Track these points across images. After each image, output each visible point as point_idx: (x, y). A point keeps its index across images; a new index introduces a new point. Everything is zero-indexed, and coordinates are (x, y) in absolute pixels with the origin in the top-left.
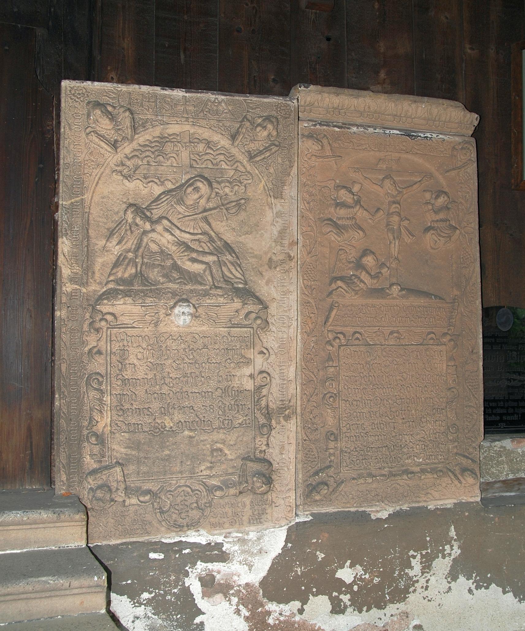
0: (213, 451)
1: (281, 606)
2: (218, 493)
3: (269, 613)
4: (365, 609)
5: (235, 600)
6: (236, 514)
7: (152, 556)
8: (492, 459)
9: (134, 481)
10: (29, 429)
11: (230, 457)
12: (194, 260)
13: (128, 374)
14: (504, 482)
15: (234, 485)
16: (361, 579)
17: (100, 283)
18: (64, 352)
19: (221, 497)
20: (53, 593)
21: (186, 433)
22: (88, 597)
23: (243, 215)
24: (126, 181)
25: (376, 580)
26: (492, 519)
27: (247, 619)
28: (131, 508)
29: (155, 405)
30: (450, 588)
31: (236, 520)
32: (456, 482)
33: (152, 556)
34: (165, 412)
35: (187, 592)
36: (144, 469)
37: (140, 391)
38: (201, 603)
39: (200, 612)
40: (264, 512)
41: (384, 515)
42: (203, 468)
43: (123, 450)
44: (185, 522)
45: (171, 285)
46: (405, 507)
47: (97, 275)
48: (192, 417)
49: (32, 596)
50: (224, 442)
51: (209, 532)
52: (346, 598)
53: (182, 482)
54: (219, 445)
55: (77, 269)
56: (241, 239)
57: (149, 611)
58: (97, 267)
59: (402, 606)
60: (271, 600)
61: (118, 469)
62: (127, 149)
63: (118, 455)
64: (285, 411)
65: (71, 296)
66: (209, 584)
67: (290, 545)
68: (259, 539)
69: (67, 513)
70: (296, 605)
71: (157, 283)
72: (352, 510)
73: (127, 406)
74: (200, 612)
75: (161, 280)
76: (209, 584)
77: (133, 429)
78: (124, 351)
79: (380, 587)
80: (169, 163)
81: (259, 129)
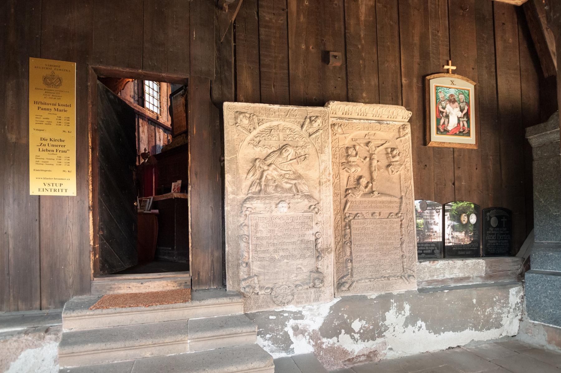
0: (297, 268)
1: (329, 339)
2: (300, 288)
3: (323, 343)
4: (366, 341)
5: (308, 337)
6: (307, 297)
7: (271, 317)
8: (421, 270)
9: (263, 283)
10: (212, 261)
11: (305, 271)
12: (287, 183)
13: (259, 235)
14: (426, 281)
15: (307, 284)
16: (364, 327)
17: (245, 194)
18: (230, 226)
19: (301, 290)
20: (234, 335)
21: (285, 261)
22: (249, 337)
23: (306, 162)
24: (255, 148)
25: (371, 327)
26: (423, 298)
27: (313, 346)
28: (262, 296)
29: (271, 249)
30: (405, 331)
31: (308, 300)
32: (406, 281)
33: (271, 317)
34: (275, 251)
35: (286, 333)
36: (267, 277)
37: (264, 242)
38: (293, 338)
39: (292, 343)
40: (320, 296)
41: (374, 297)
42: (293, 276)
43: (258, 269)
44: (286, 302)
45: (276, 194)
46: (383, 293)
47: (243, 190)
48: (288, 254)
49: (225, 336)
50: (302, 264)
51: (296, 306)
52: (357, 336)
53: (284, 283)
54: (300, 266)
55: (235, 188)
56: (307, 172)
57: (270, 343)
58: (243, 187)
59: (382, 340)
60: (324, 337)
61: (256, 278)
62: (255, 133)
63: (255, 272)
64: (327, 250)
65: (233, 200)
66: (296, 329)
67: (332, 312)
68: (318, 309)
69: (236, 299)
70: (335, 339)
71: (271, 193)
72: (359, 294)
73: (258, 249)
74: (292, 343)
75: (273, 192)
76: (296, 329)
77: (261, 259)
78: (257, 225)
79: (373, 330)
80: (274, 139)
81: (313, 122)
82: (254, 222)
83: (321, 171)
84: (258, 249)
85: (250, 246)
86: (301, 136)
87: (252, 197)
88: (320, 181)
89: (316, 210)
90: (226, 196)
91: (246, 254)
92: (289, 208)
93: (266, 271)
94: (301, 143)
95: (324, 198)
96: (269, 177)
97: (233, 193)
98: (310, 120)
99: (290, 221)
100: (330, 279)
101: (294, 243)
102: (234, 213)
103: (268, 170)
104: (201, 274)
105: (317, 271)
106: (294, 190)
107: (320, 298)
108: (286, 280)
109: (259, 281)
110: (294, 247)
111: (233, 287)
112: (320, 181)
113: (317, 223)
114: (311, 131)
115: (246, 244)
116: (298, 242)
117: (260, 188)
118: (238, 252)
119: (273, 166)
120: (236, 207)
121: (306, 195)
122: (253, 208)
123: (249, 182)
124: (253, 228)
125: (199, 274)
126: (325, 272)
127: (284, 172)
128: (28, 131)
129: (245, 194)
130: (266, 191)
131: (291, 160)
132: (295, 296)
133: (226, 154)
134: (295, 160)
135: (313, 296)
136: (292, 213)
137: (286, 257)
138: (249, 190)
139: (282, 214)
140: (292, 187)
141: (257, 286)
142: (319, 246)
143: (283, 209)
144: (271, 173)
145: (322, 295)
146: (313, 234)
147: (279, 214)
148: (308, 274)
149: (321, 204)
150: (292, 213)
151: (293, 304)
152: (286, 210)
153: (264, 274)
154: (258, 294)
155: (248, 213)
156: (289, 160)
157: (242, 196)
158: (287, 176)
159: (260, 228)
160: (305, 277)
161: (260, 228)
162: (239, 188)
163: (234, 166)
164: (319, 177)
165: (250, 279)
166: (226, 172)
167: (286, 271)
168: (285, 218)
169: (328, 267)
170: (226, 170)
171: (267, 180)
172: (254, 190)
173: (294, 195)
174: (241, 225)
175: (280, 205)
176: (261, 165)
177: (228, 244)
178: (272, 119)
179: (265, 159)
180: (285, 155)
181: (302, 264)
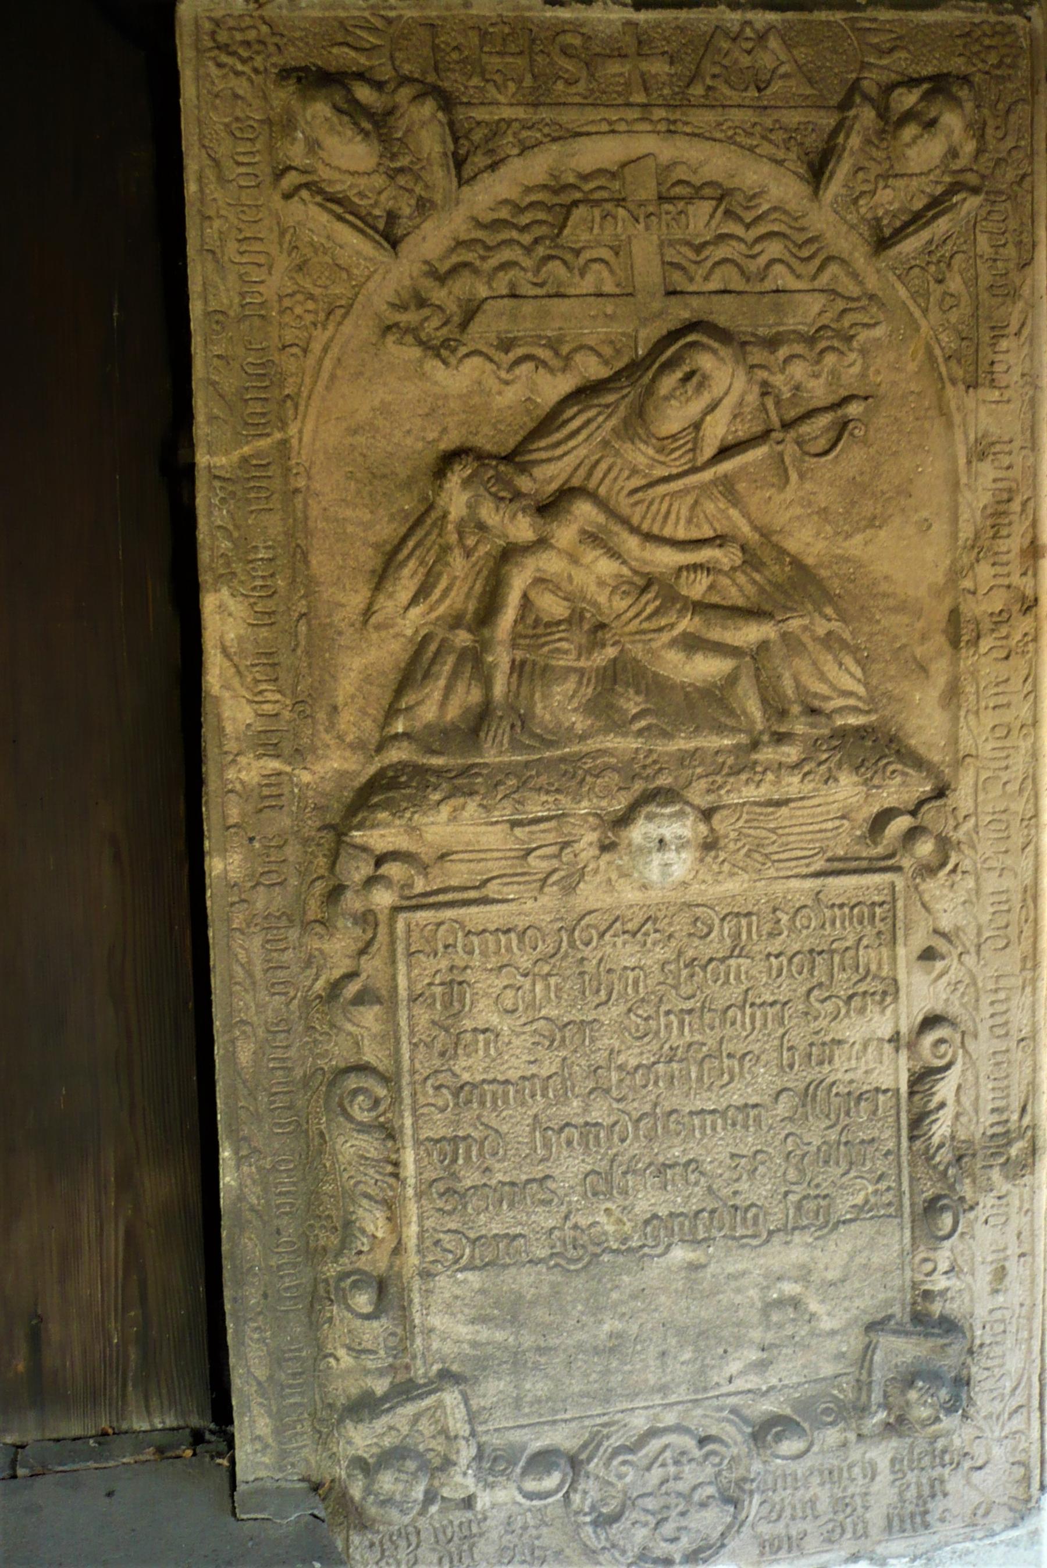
6: (841, 1504)
9: (504, 1430)
11: (826, 1324)
12: (692, 644)
13: (470, 1067)
17: (359, 746)
21: (680, 1254)
23: (852, 459)
24: (433, 366)
29: (570, 1167)
34: (601, 1185)
40: (936, 1489)
43: (464, 1331)
47: (346, 718)
53: (670, 1418)
54: (790, 1288)
55: (274, 700)
56: (854, 547)
58: (346, 686)
63: (448, 1348)
65: (268, 797)
71: (570, 735)
75: (580, 722)
78: (455, 987)
81: (910, 131)
82: (432, 968)
83: (966, 532)
84: (470, 1178)
85: (409, 1157)
86: (810, 251)
87: (420, 771)
88: (954, 615)
89: (925, 848)
90: (210, 770)
91: (373, 1221)
92: (710, 845)
93: (528, 1340)
94: (809, 310)
95: (986, 749)
96: (552, 606)
97: (266, 743)
98: (883, 113)
99: (715, 946)
100: (1014, 1363)
101: (747, 1113)
102: (279, 900)
103: (542, 543)
104: (54, 1331)
105: (928, 1318)
106: (754, 708)
107: (936, 1507)
108: (681, 1393)
109: (472, 1418)
110: (750, 1143)
111: (283, 1454)
112: (954, 615)
113: (928, 955)
114: (890, 200)
115: (370, 1145)
116: (782, 1108)
117: (475, 696)
118: (313, 1198)
119: (584, 510)
120: (292, 852)
121: (842, 734)
122: (426, 853)
123: (385, 652)
124: (423, 1016)
125: (36, 1338)
126: (981, 1312)
127: (666, 558)
128: (178, 477)
129: (359, 746)
130: (524, 720)
131: (725, 452)
132: (753, 1507)
133: (201, 428)
134: (759, 452)
135: (883, 1493)
136: (731, 886)
137: (686, 1226)
138: (392, 712)
139: (654, 896)
140: (732, 679)
141: (466, 1453)
142: (941, 1128)
143: (666, 858)
144: (574, 569)
145: (955, 1483)
146: (895, 1039)
147: (630, 895)
148: (853, 1343)
149: (962, 797)
150: (731, 886)
151: (733, 1556)
152: (681, 864)
153: (517, 1362)
154: (468, 1502)
155: (383, 898)
156: (709, 451)
157: (334, 765)
158: (697, 588)
159: (485, 1014)
160: (828, 1369)
161: (485, 1014)
162: (310, 701)
163: (274, 525)
164: (955, 574)
165: (410, 1409)
166: (205, 578)
167: (681, 1332)
168: (681, 925)
169: (1000, 1273)
170: (204, 556)
171: (533, 627)
172: (428, 713)
173: (755, 745)
174: (335, 987)
175: (639, 832)
176: (488, 513)
177: (232, 1132)
178: (569, 117)
179: (515, 458)
180: (674, 418)
181: (804, 1274)
